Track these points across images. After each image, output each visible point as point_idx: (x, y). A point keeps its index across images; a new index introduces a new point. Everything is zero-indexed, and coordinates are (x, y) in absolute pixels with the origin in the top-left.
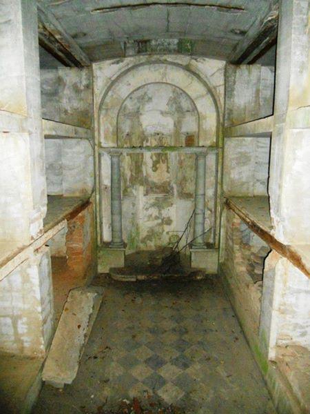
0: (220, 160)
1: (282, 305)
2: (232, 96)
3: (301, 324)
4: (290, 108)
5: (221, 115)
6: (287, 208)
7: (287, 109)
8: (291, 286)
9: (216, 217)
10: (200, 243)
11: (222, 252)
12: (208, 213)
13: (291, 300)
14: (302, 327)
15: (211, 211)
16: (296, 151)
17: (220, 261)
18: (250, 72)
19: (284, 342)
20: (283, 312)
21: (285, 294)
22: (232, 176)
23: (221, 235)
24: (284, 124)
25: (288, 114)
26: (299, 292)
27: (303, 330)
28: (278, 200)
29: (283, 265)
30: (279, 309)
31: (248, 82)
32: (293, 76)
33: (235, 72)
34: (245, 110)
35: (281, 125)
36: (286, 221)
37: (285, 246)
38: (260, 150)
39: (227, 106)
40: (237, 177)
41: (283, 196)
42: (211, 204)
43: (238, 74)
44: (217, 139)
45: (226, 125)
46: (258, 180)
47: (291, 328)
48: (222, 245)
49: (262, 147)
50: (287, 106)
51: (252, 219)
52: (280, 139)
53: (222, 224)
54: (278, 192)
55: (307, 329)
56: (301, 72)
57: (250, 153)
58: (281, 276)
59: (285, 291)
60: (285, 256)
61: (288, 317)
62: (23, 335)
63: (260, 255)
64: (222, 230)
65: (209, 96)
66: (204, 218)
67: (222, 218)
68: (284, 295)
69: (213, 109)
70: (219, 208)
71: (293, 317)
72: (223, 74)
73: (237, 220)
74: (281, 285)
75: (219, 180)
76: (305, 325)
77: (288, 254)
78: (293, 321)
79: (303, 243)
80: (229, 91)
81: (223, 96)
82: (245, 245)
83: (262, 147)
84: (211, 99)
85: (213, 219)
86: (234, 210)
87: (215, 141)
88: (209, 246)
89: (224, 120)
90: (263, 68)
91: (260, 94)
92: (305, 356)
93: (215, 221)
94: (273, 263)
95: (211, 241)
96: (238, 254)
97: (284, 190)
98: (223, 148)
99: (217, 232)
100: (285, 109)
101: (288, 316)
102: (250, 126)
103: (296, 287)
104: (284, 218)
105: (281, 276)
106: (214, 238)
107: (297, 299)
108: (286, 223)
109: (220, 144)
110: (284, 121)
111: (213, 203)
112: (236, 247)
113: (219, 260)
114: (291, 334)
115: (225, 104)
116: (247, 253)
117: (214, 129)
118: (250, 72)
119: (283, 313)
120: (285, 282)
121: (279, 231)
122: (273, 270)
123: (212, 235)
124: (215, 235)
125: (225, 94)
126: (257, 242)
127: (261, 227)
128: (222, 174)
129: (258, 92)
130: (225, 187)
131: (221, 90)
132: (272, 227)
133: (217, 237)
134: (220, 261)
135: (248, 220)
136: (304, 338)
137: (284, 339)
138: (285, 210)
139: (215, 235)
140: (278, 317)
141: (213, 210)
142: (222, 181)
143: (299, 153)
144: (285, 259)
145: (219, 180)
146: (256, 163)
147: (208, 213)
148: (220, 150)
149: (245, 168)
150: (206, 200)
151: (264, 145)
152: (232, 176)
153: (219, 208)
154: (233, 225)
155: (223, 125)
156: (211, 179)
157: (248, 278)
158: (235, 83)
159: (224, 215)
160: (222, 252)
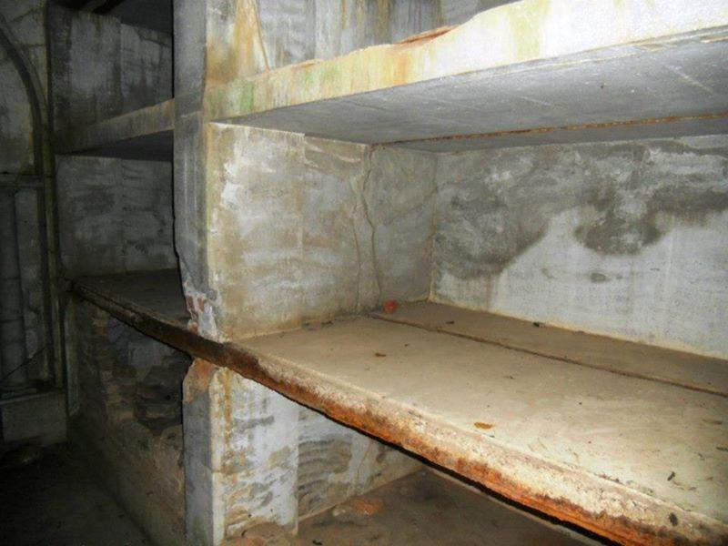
0: (49, 203)
1: (228, 458)
2: (64, 70)
3: (262, 482)
4: (209, 84)
5: (42, 107)
6: (219, 273)
7: (204, 85)
8: (238, 417)
9: (49, 323)
10: (20, 385)
11: (74, 394)
12: (30, 317)
13: (242, 442)
14: (264, 488)
15: (36, 311)
16: (225, 165)
17: (72, 413)
18: (99, 29)
19: (238, 526)
20: (229, 471)
21: (230, 436)
22: (79, 234)
23: (68, 357)
24: (199, 112)
25: (206, 94)
26: (252, 424)
27: (265, 493)
28: (201, 257)
29: (221, 382)
30: (224, 465)
31: (97, 49)
32: (210, 24)
33: (69, 24)
34: (94, 99)
35: (193, 114)
36: (219, 298)
37: (222, 345)
38: (129, 183)
39: (55, 89)
40: (88, 236)
41: (210, 250)
42: (36, 298)
43: (74, 29)
44: (38, 155)
45: (56, 128)
46: (131, 243)
47: (246, 495)
48: (72, 378)
49: (132, 178)
50: (204, 79)
51: (141, 311)
52: (191, 143)
53: (67, 334)
54: (197, 244)
55: (271, 488)
56: (224, 18)
57: (110, 187)
58: (221, 402)
59: (228, 429)
60: (223, 364)
61: (240, 477)
62: (150, 70)
63: (152, 384)
64: (68, 348)
65: (11, 65)
66: (23, 329)
67: (66, 324)
68: (227, 439)
69: (22, 94)
70: (56, 305)
71: (248, 475)
72: (41, 23)
73: (101, 321)
74: (223, 422)
75: (51, 244)
76: (268, 482)
77: (229, 360)
78: (249, 481)
79: (249, 335)
80: (58, 61)
81: (44, 69)
82: (122, 367)
83: (132, 178)
84: (17, 73)
85: (44, 328)
86: (93, 302)
87: (32, 162)
88: (43, 386)
89: (50, 119)
90: (125, 29)
91: (123, 76)
92: (277, 537)
93: (50, 333)
94: (201, 384)
95: (45, 375)
96: (112, 389)
97: (210, 237)
98: (53, 176)
99: (58, 354)
100: (199, 83)
101: (239, 474)
102: (118, 123)
103: (246, 418)
104: (215, 292)
105: (221, 402)
106: (52, 369)
107: (251, 437)
108: (219, 301)
109: (46, 168)
110: (199, 106)
111: (40, 295)
112: (107, 375)
113: (67, 412)
114: (246, 506)
115: (50, 85)
116: (129, 383)
117: (28, 137)
118: (99, 29)
119: (230, 473)
120: (228, 413)
121: (207, 319)
122: (205, 397)
123: (46, 364)
124: (52, 360)
125: (49, 65)
126: (151, 354)
127: (163, 321)
128: (56, 233)
129: (117, 70)
130: (65, 258)
131: (40, 56)
132: (187, 319)
133: (58, 366)
134: (72, 413)
135: (131, 314)
136: (269, 507)
137: (238, 521)
138: (216, 278)
139: (52, 360)
140: (223, 483)
141: (42, 309)
142: (57, 245)
143: (231, 169)
144: (223, 370)
145: (51, 244)
146: (125, 208)
147: (30, 317)
148: (48, 181)
149: (105, 219)
150: (24, 289)
151: (135, 175)
152: (79, 234)
153: (56, 305)
154: (93, 333)
155: (50, 129)
156: (30, 244)
157: (141, 430)
158: (69, 43)
159: (69, 315)
160: (74, 394)
